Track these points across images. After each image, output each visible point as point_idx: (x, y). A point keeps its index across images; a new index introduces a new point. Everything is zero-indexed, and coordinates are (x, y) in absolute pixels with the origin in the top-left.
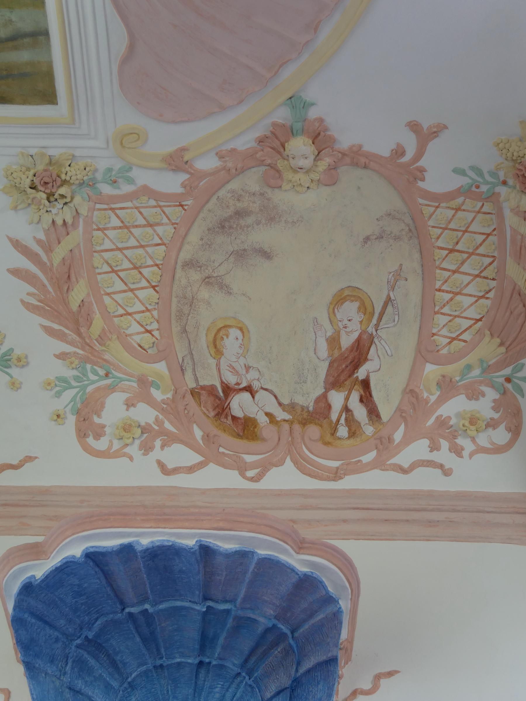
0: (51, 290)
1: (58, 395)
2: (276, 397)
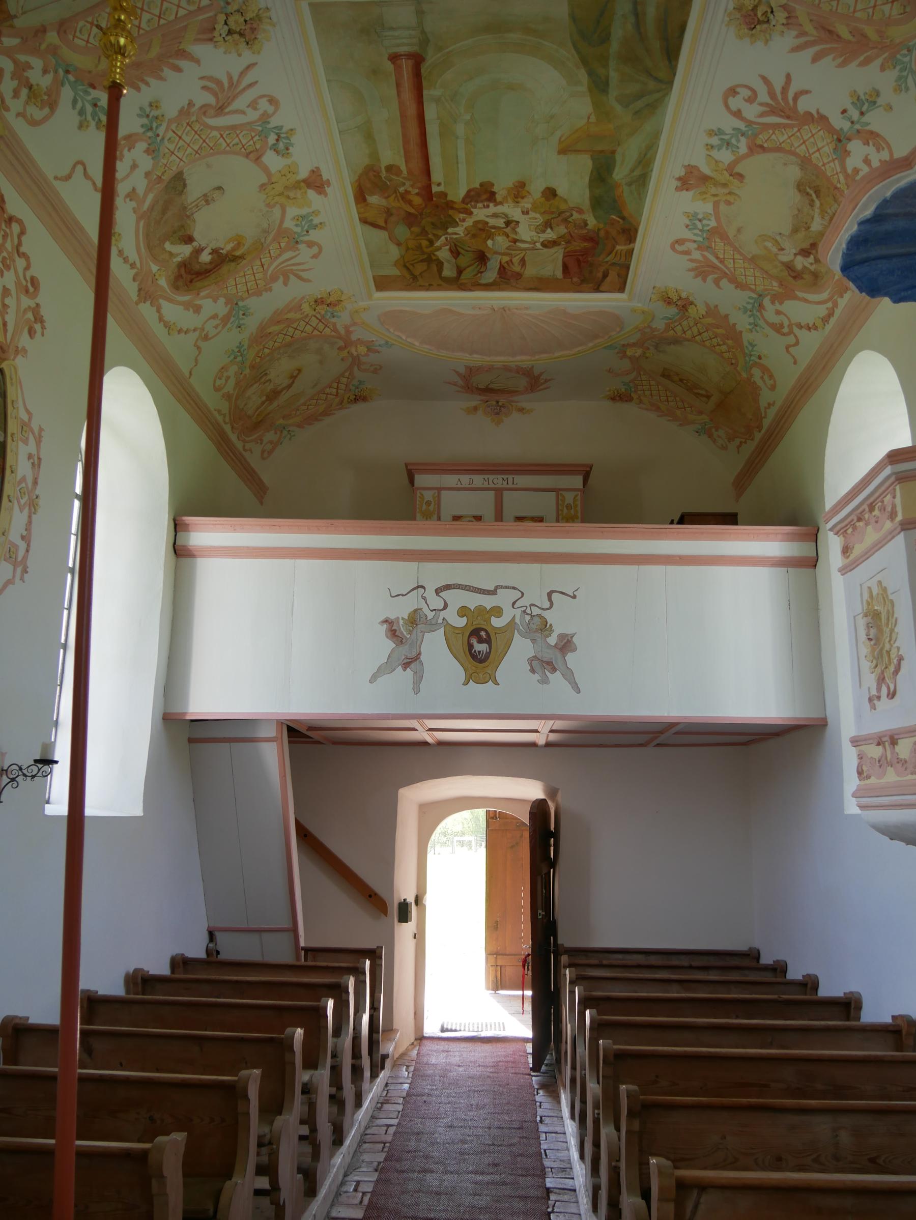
1: (907, 89)
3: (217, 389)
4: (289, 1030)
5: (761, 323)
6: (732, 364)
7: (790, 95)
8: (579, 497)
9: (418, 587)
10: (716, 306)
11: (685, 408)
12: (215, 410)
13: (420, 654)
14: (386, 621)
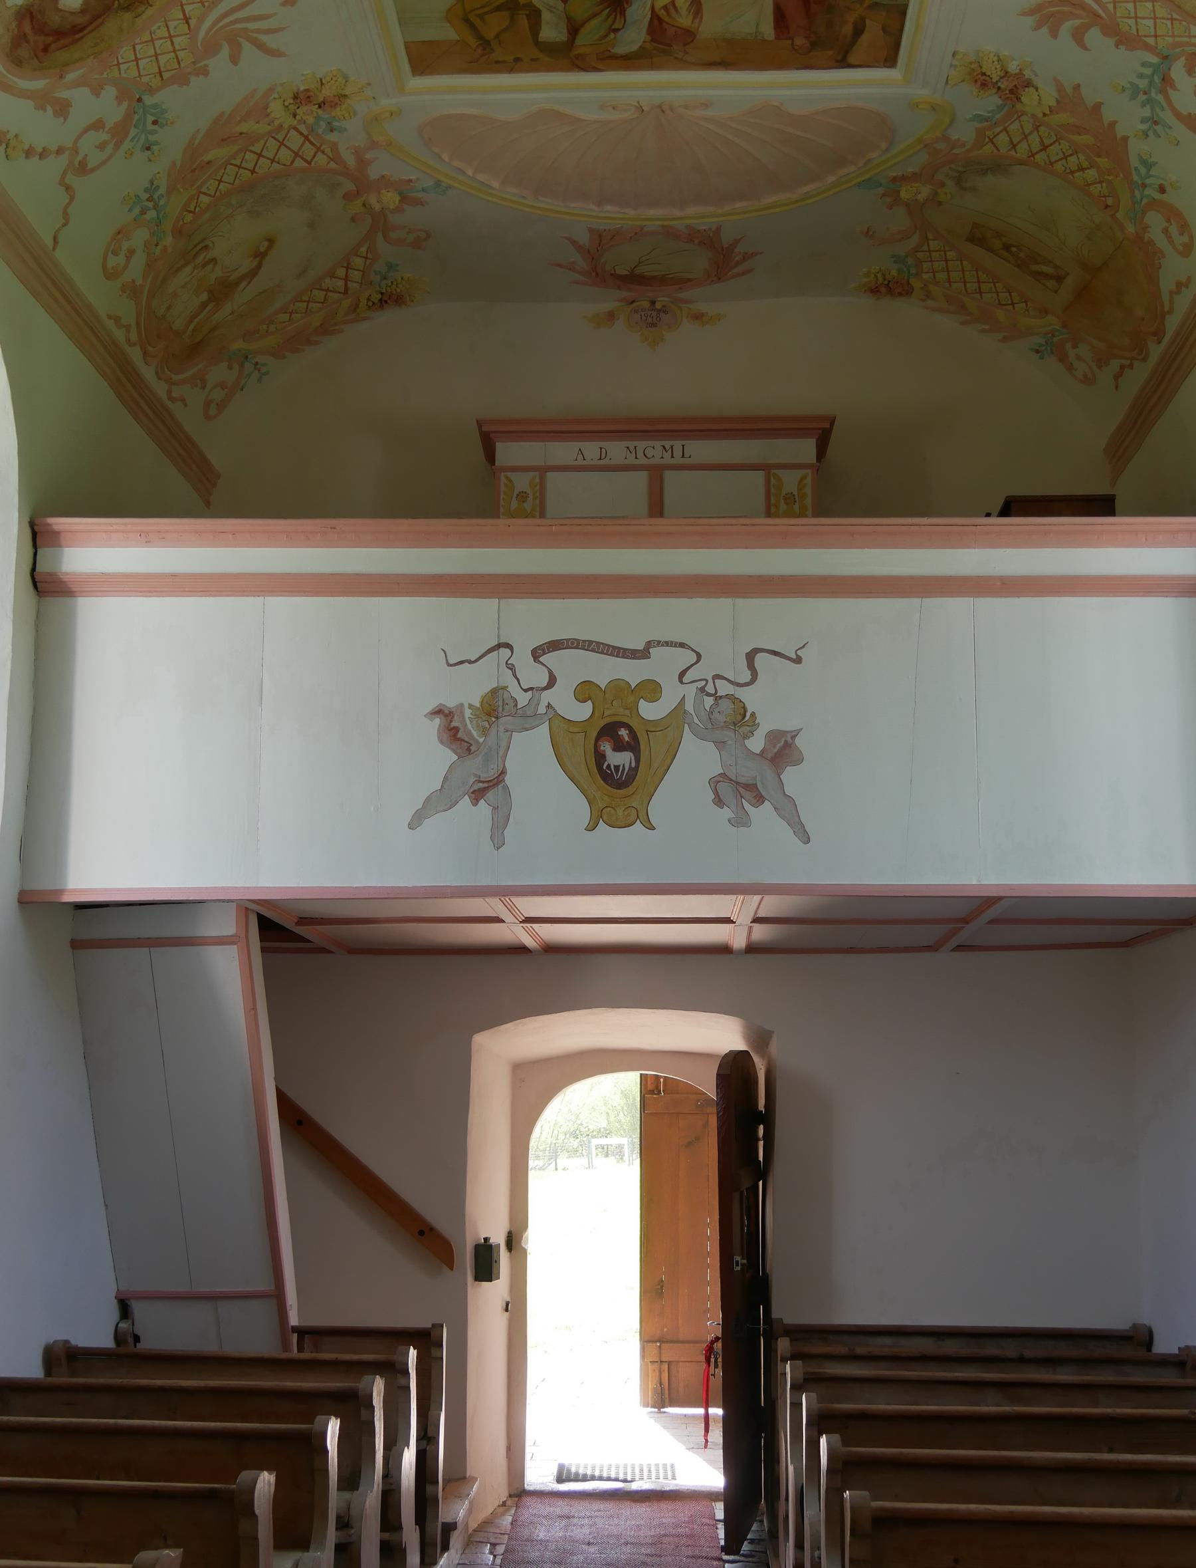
3: (111, 275)
4: (245, 1476)
6: (1107, 207)
8: (809, 481)
9: (499, 646)
10: (1077, 87)
11: (1013, 304)
12: (109, 317)
13: (503, 772)
14: (438, 712)
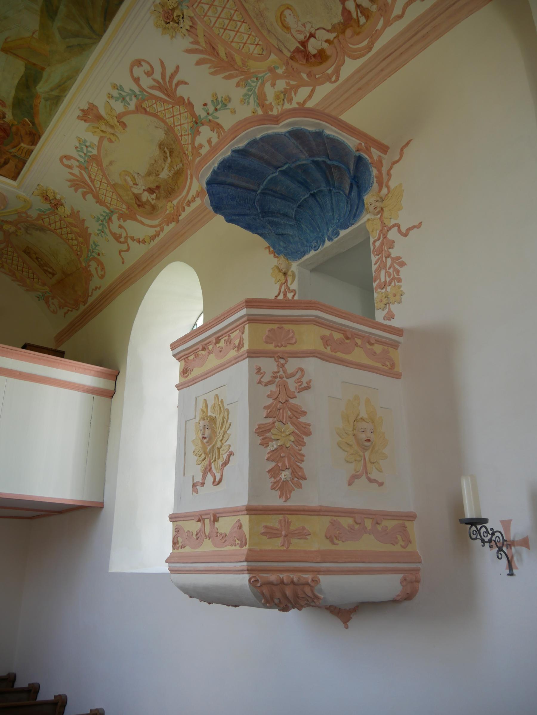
0: (214, 59)
1: (248, 103)
2: (324, 29)
5: (107, 231)
6: (78, 255)
7: (175, 81)
10: (78, 212)
11: (34, 279)
